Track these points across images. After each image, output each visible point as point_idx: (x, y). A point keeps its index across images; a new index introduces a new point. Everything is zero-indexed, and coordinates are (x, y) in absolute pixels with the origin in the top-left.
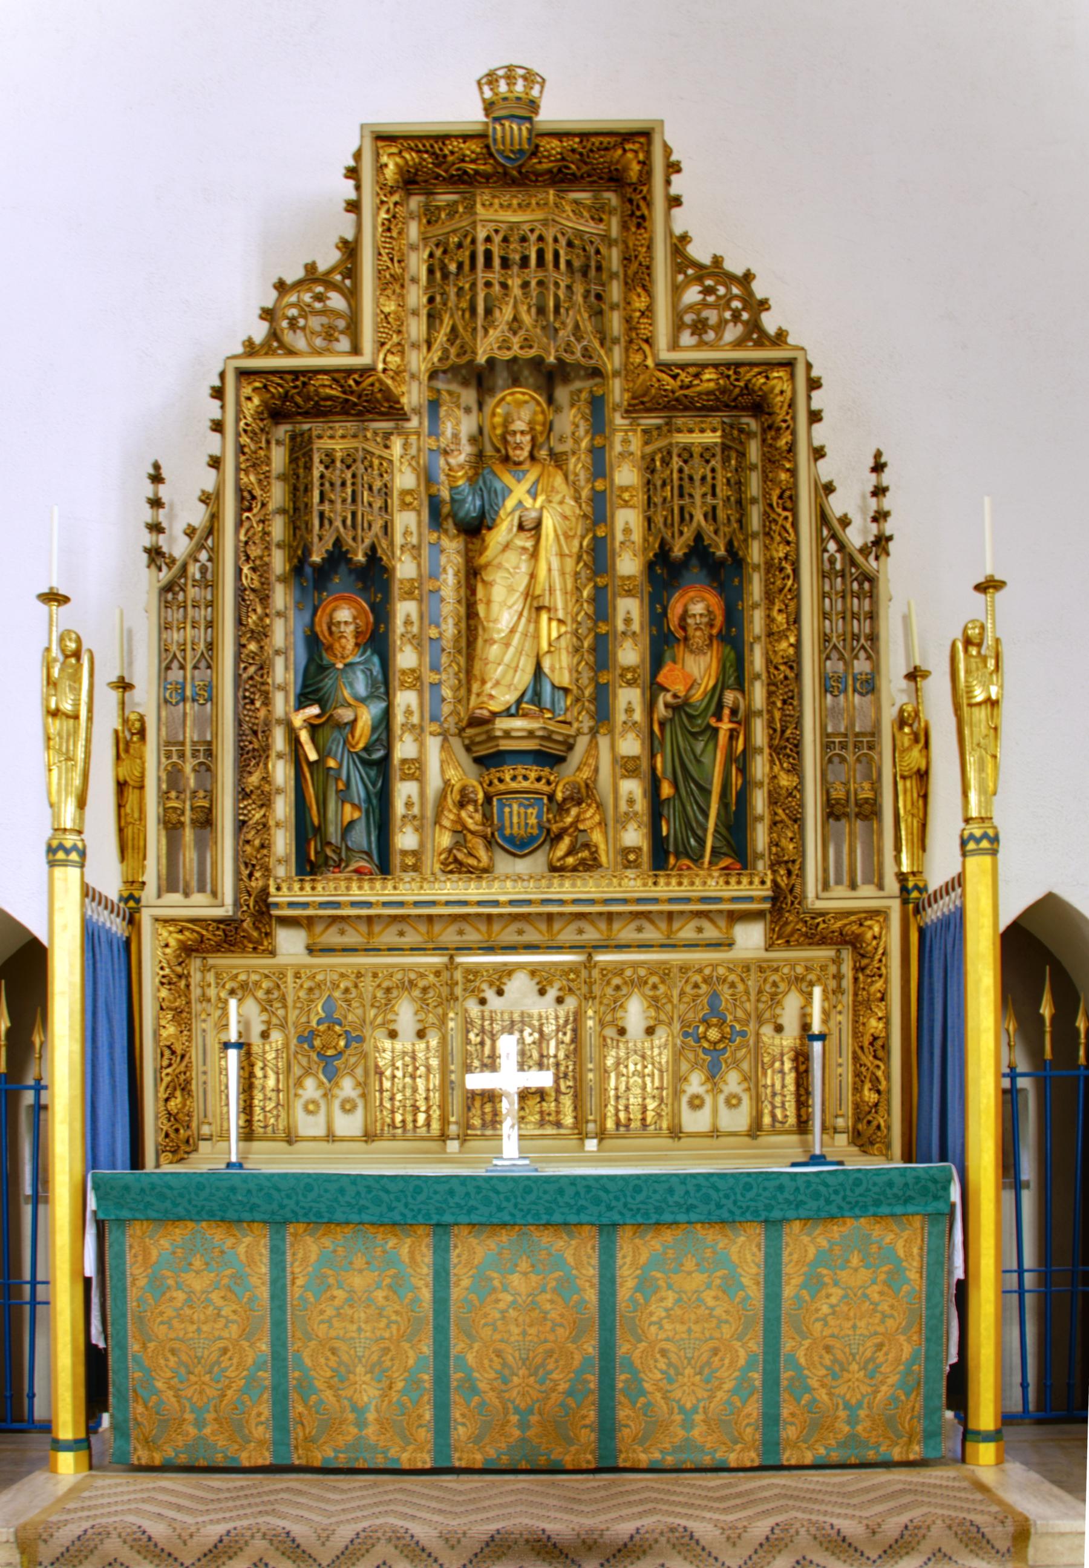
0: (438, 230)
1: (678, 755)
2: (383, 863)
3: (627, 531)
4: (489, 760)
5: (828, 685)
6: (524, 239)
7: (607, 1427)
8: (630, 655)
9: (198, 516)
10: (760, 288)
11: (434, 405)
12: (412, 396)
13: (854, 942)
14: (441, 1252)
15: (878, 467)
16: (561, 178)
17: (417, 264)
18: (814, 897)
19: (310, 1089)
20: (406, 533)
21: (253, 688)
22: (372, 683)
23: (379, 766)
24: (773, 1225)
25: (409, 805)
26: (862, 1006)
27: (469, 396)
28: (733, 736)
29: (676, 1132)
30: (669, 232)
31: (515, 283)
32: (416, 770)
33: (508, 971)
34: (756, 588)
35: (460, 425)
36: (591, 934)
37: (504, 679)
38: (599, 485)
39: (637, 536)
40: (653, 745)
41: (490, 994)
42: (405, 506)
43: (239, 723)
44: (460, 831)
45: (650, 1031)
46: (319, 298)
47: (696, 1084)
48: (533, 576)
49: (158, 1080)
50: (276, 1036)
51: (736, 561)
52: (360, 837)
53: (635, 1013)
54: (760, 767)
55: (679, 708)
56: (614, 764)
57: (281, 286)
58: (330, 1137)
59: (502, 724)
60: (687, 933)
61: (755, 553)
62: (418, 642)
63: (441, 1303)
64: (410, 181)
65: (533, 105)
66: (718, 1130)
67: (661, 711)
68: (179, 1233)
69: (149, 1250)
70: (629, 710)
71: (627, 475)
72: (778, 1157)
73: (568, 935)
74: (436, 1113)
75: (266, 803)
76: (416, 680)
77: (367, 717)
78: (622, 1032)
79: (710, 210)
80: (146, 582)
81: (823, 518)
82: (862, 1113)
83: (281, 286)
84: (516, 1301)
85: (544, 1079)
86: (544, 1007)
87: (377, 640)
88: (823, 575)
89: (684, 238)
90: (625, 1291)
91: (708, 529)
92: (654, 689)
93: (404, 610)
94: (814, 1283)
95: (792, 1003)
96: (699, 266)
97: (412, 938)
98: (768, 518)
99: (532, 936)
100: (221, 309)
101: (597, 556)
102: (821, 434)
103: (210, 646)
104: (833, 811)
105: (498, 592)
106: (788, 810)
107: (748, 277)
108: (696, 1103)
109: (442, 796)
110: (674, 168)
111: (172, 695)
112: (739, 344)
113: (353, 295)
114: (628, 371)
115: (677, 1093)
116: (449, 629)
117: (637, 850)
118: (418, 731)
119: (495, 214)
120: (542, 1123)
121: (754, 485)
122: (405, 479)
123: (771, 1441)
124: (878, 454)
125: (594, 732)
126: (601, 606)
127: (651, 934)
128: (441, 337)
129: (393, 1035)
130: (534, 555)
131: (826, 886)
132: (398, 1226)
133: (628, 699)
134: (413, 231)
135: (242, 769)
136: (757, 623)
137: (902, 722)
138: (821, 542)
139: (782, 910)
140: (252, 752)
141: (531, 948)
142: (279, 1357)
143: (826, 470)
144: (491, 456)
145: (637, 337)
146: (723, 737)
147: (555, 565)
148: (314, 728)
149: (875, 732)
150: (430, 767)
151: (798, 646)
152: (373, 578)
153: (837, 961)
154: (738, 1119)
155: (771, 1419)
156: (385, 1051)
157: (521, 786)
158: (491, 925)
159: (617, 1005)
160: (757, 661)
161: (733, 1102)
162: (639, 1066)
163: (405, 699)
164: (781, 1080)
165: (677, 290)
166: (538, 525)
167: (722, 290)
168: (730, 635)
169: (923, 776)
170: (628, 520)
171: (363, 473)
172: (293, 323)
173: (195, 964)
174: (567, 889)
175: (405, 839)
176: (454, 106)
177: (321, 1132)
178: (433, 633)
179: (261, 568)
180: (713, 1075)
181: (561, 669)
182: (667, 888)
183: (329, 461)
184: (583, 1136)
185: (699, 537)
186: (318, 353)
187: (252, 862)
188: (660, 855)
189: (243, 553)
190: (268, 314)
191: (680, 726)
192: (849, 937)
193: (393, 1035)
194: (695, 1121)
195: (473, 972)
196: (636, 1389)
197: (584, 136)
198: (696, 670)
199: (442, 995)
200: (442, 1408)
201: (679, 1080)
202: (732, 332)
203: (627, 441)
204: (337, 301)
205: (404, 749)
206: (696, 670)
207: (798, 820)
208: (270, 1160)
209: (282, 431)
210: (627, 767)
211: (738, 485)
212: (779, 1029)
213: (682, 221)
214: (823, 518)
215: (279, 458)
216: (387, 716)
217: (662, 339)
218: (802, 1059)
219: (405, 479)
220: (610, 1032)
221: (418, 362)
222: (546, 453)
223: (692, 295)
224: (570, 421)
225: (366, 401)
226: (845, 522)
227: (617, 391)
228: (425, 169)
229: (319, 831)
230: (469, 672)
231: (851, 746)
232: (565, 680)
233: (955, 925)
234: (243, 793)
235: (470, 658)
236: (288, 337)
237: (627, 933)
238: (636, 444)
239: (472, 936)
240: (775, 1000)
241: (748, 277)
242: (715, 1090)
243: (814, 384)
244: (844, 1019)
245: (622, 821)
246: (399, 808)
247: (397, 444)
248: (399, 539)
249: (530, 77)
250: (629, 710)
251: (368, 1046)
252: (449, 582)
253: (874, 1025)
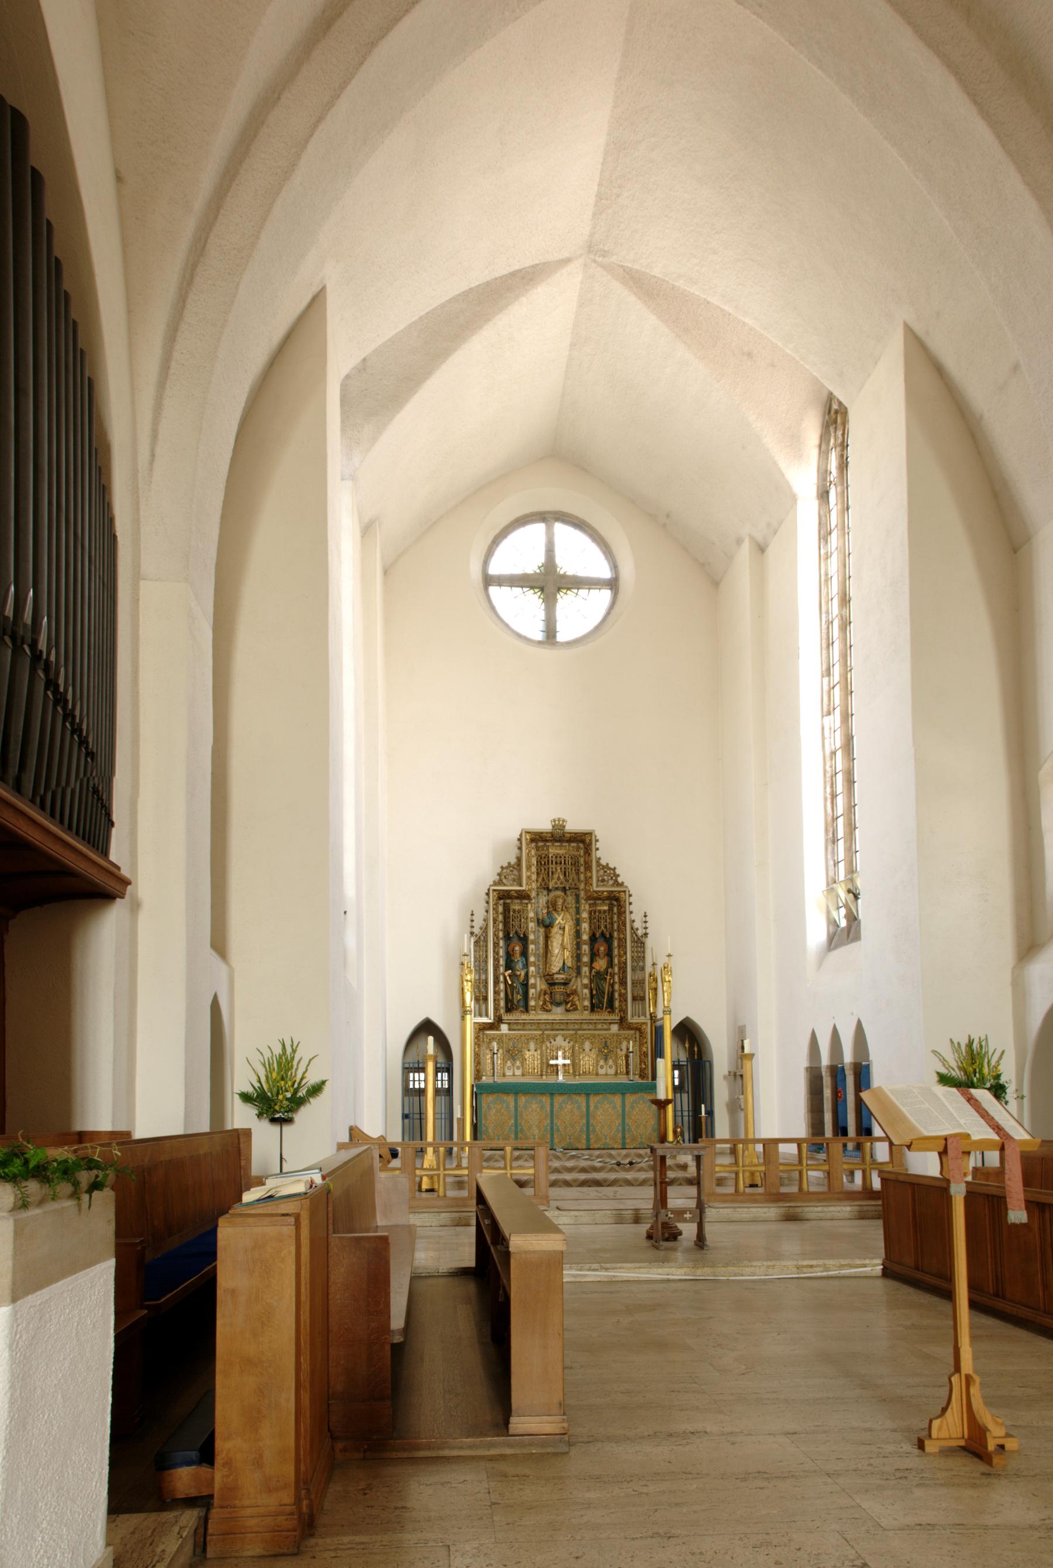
0: (539, 853)
2: (527, 1009)
4: (552, 984)
5: (633, 970)
7: (588, 1140)
10: (617, 871)
12: (533, 894)
13: (639, 1030)
14: (552, 1099)
16: (569, 841)
17: (534, 861)
18: (630, 1019)
19: (509, 1063)
23: (526, 986)
24: (623, 1094)
26: (641, 1045)
27: (545, 892)
29: (597, 1074)
32: (534, 986)
34: (616, 943)
35: (543, 900)
36: (577, 1027)
37: (556, 966)
40: (591, 981)
44: (545, 1002)
47: (602, 1063)
51: (611, 936)
52: (522, 1003)
53: (587, 1045)
54: (617, 987)
56: (581, 985)
57: (502, 868)
59: (556, 976)
60: (599, 1026)
61: (616, 934)
62: (535, 955)
63: (552, 1111)
66: (607, 1073)
68: (495, 1096)
69: (487, 1100)
71: (585, 915)
72: (623, 1079)
73: (571, 1027)
76: (534, 964)
77: (523, 973)
79: (606, 852)
81: (632, 928)
82: (642, 1070)
83: (502, 868)
84: (570, 1110)
85: (568, 1062)
86: (565, 1044)
87: (524, 953)
90: (591, 1109)
92: (591, 968)
93: (531, 947)
94: (632, 1107)
95: (624, 1045)
97: (534, 1027)
98: (618, 926)
101: (578, 934)
102: (632, 908)
104: (634, 999)
105: (555, 944)
106: (623, 997)
108: (602, 1067)
110: (597, 841)
112: (613, 885)
114: (586, 891)
116: (541, 951)
118: (535, 977)
119: (554, 850)
121: (615, 918)
122: (531, 915)
123: (624, 1143)
126: (578, 946)
127: (591, 1027)
128: (540, 880)
130: (563, 935)
132: (542, 1094)
133: (585, 970)
135: (495, 987)
136: (616, 952)
137: (650, 976)
139: (623, 1022)
142: (516, 1125)
143: (633, 917)
144: (552, 906)
145: (588, 881)
147: (568, 938)
148: (510, 976)
149: (644, 980)
152: (524, 940)
154: (612, 1071)
155: (624, 1138)
156: (527, 1054)
157: (558, 992)
158: (553, 1025)
159: (583, 1043)
160: (616, 961)
161: (611, 1067)
162: (588, 1060)
163: (532, 969)
164: (622, 1062)
165: (598, 871)
168: (609, 954)
169: (656, 989)
170: (585, 926)
175: (532, 1003)
176: (546, 826)
180: (606, 1060)
181: (569, 963)
182: (595, 1017)
183: (514, 911)
188: (593, 1008)
191: (598, 977)
192: (638, 1029)
194: (602, 1072)
196: (594, 1131)
198: (601, 964)
199: (541, 1041)
200: (552, 1135)
201: (598, 1062)
202: (611, 882)
205: (532, 981)
207: (626, 1001)
208: (498, 1079)
209: (501, 902)
210: (585, 986)
211: (612, 918)
213: (599, 854)
214: (632, 928)
217: (594, 885)
218: (627, 1057)
219: (531, 915)
221: (534, 885)
222: (564, 908)
224: (571, 899)
227: (582, 894)
228: (537, 838)
229: (512, 1001)
231: (639, 983)
233: (662, 1027)
237: (585, 1027)
238: (587, 907)
239: (548, 1027)
240: (620, 1043)
243: (630, 896)
244: (637, 1048)
245: (584, 999)
246: (530, 995)
249: (564, 821)
252: (541, 939)
253: (644, 1049)
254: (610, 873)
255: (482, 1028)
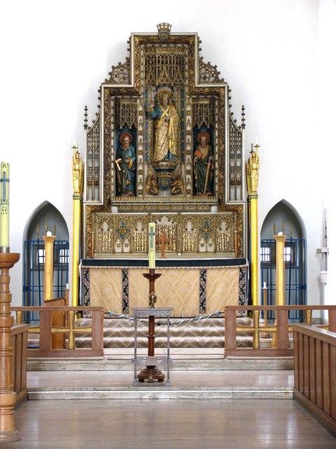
0: (148, 54)
1: (199, 171)
3: (189, 121)
4: (158, 171)
6: (167, 57)
8: (189, 148)
9: (95, 118)
10: (218, 70)
11: (146, 91)
15: (243, 109)
17: (143, 60)
19: (118, 242)
20: (141, 120)
21: (107, 156)
22: (133, 154)
25: (141, 180)
28: (211, 166)
29: (198, 252)
30: (198, 56)
31: (164, 67)
32: (142, 172)
33: (162, 216)
37: (162, 153)
38: (183, 109)
39: (191, 122)
40: (194, 168)
41: (158, 221)
42: (140, 115)
43: (105, 163)
45: (192, 229)
46: (122, 71)
47: (202, 241)
48: (168, 131)
49: (86, 239)
50: (111, 230)
53: (189, 226)
55: (199, 160)
58: (123, 252)
62: (143, 144)
64: (141, 43)
65: (169, 30)
67: (195, 161)
69: (96, 275)
70: (189, 160)
71: (189, 108)
74: (146, 247)
75: (110, 180)
76: (142, 153)
77: (131, 161)
78: (186, 229)
79: (208, 53)
80: (85, 132)
81: (230, 120)
87: (134, 143)
88: (230, 132)
89: (202, 58)
91: (206, 122)
93: (140, 137)
96: (205, 65)
99: (167, 208)
100: (101, 73)
101: (182, 125)
103: (98, 146)
104: (231, 183)
105: (160, 135)
106: (222, 181)
107: (216, 67)
108: (202, 245)
109: (148, 177)
111: (89, 157)
113: (129, 70)
115: (198, 243)
116: (149, 140)
117: (190, 190)
118: (143, 164)
119: (160, 52)
120: (169, 249)
122: (140, 109)
124: (243, 106)
125: (181, 164)
129: (137, 230)
131: (230, 199)
133: (188, 157)
134: (142, 53)
138: (230, 125)
139: (220, 203)
140: (107, 169)
141: (166, 211)
144: (158, 103)
146: (209, 167)
148: (120, 164)
150: (145, 170)
151: (224, 148)
152: (133, 132)
153: (233, 215)
157: (164, 179)
159: (185, 223)
161: (210, 245)
163: (140, 157)
165: (200, 70)
166: (169, 121)
167: (210, 70)
168: (211, 143)
170: (189, 118)
171: (132, 109)
172: (116, 76)
173: (93, 214)
174: (175, 199)
175: (140, 188)
176: (152, 30)
177: (120, 251)
178: (146, 142)
179: (109, 130)
180: (206, 239)
182: (196, 200)
184: (178, 252)
185: (204, 124)
186: (122, 83)
187: (106, 193)
188: (195, 192)
189: (105, 127)
190: (110, 74)
191: (199, 164)
193: (137, 230)
195: (154, 216)
197: (180, 36)
198: (203, 151)
202: (212, 79)
203: (189, 101)
204: (125, 71)
206: (203, 151)
207: (224, 185)
209: (113, 97)
210: (188, 172)
211: (214, 111)
212: (221, 229)
214: (230, 120)
215: (112, 104)
216: (136, 161)
217: (196, 83)
220: (184, 229)
223: (203, 70)
224: (177, 94)
225: (131, 93)
226: (235, 121)
229: (121, 185)
230: (154, 150)
232: (175, 153)
234: (105, 178)
235: (154, 147)
236: (115, 79)
238: (191, 101)
241: (216, 67)
242: (207, 242)
245: (187, 184)
246: (139, 181)
247: (138, 101)
248: (139, 122)
249: (168, 25)
250: (189, 160)
251: (131, 232)
254: (211, 71)
255: (95, 210)
